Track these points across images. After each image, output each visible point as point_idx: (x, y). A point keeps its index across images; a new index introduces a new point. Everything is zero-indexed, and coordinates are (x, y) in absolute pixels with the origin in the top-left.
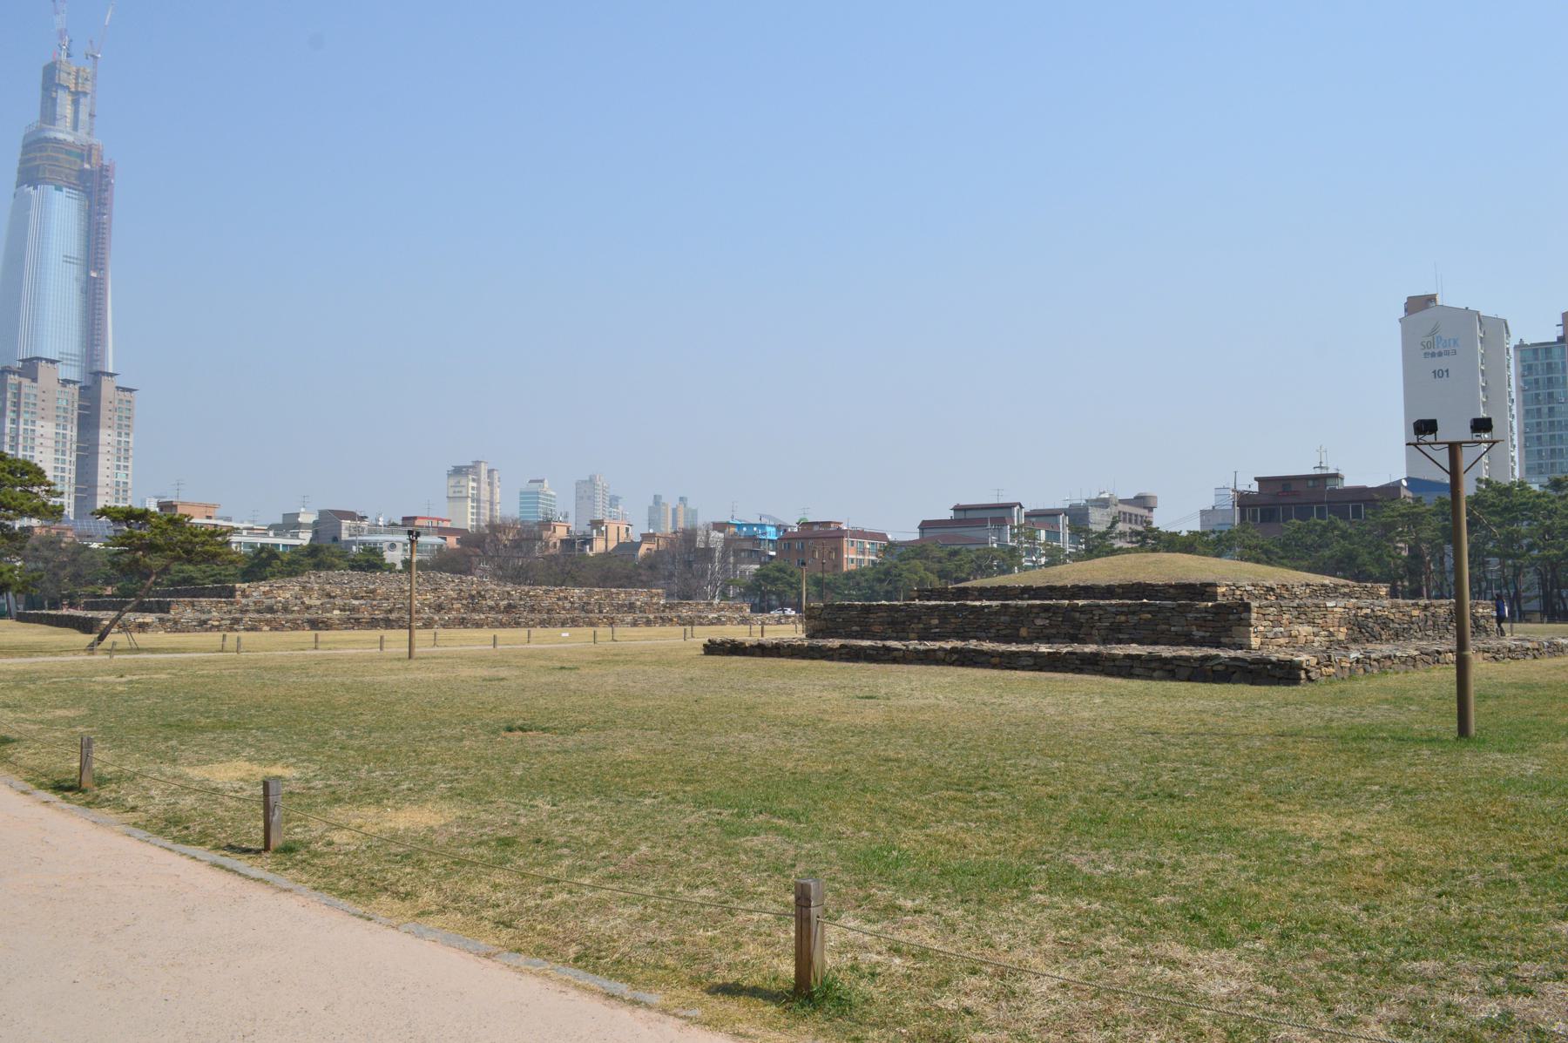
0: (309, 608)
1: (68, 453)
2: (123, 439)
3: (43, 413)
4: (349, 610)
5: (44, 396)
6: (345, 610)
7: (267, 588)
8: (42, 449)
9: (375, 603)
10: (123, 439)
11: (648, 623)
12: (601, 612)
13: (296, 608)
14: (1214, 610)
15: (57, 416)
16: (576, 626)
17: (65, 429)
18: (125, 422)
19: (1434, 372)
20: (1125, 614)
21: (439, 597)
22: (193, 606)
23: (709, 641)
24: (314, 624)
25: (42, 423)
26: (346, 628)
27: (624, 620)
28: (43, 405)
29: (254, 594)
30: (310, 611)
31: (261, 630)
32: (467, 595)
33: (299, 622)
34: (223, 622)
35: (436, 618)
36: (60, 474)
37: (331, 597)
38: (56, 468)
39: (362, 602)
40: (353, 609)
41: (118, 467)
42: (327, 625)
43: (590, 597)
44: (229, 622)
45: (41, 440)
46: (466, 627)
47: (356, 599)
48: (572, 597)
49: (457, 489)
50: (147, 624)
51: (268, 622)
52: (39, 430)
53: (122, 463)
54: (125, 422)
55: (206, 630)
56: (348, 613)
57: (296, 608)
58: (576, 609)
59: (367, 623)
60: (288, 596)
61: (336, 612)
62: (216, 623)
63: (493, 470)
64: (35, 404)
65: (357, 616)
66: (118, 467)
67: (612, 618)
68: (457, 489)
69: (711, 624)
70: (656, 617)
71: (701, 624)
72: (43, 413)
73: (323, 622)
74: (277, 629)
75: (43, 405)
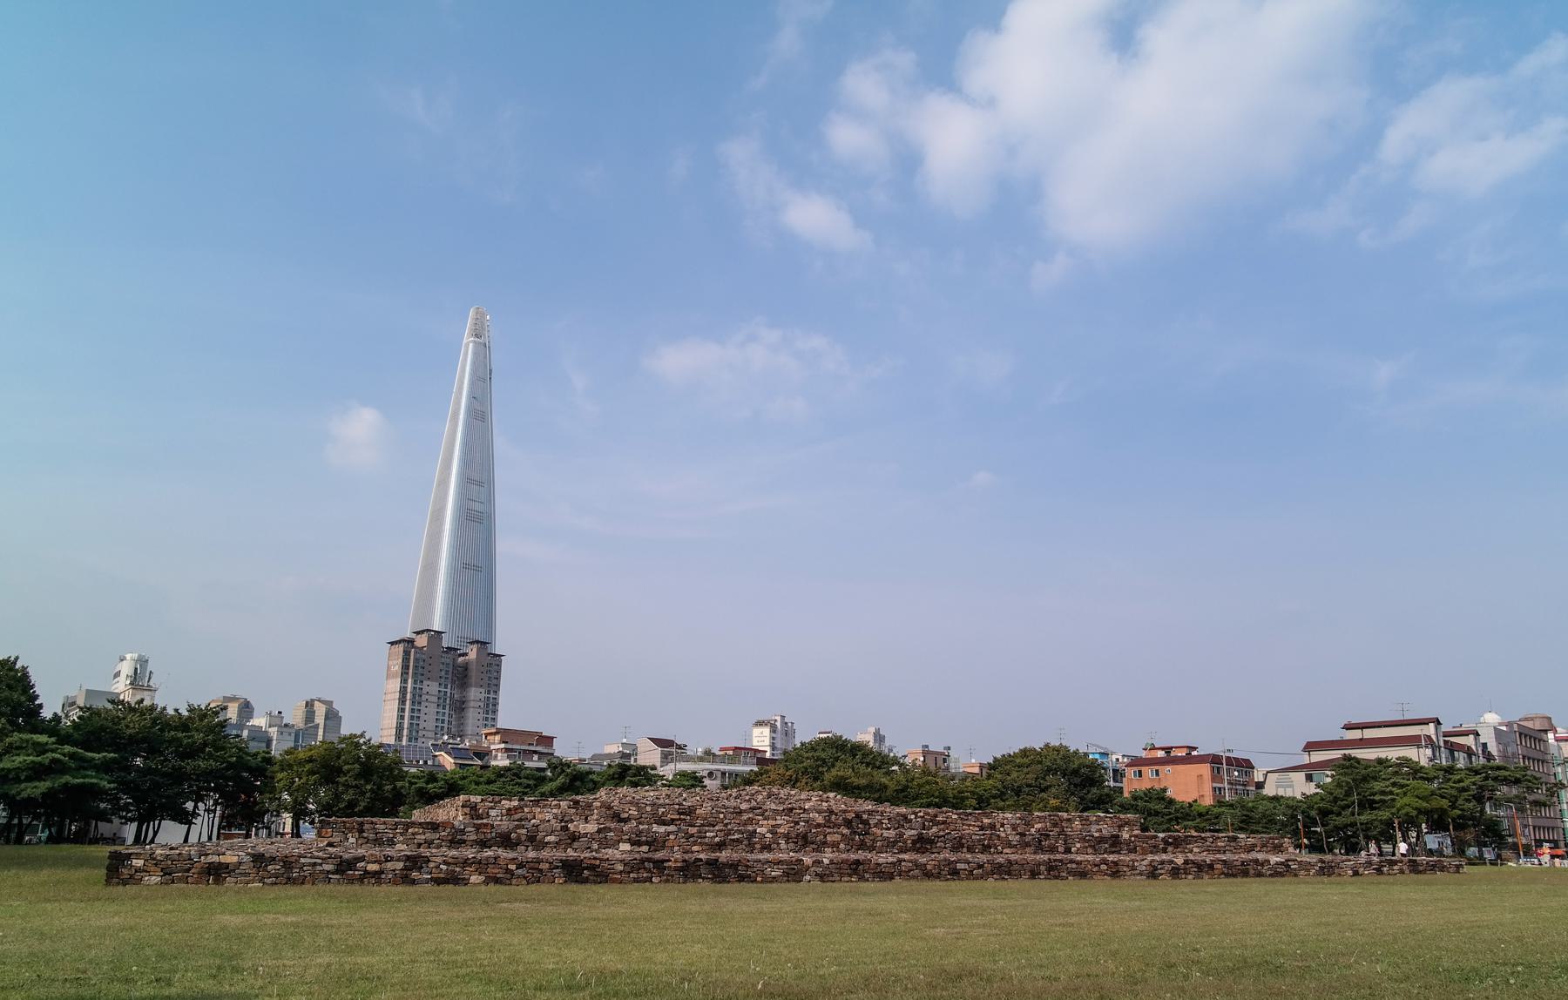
0: (574, 838)
1: (448, 707)
2: (492, 695)
3: (429, 675)
4: (647, 843)
5: (430, 661)
6: (639, 844)
7: (516, 803)
8: (427, 704)
9: (693, 830)
10: (492, 695)
11: (1176, 872)
12: (1068, 851)
13: (551, 838)
14: (450, 838)
15: (441, 677)
16: (1056, 877)
17: (446, 687)
18: (495, 681)
19: (949, 748)
20: (1220, 830)
21: (797, 823)
22: (361, 831)
23: (38, 696)
24: (574, 872)
25: (428, 683)
26: (636, 881)
27: (1133, 868)
28: (430, 668)
29: (493, 813)
30: (576, 845)
31: (466, 882)
32: (840, 821)
33: (545, 866)
34: (389, 865)
35: (808, 860)
36: (440, 725)
37: (621, 820)
38: (437, 719)
39: (672, 828)
40: (655, 843)
41: (487, 719)
42: (597, 874)
43: (1028, 824)
44: (400, 865)
45: (424, 733)
46: (862, 879)
47: (664, 823)
48: (1003, 825)
49: (760, 739)
50: (227, 865)
51: (481, 866)
52: (426, 689)
53: (490, 716)
54: (495, 681)
55: (351, 881)
56: (645, 848)
57: (551, 838)
58: (1028, 845)
59: (676, 869)
60: (548, 816)
61: (625, 847)
62: (373, 867)
63: (313, 700)
64: (423, 675)
65: (659, 855)
66: (487, 719)
67: (1116, 863)
68: (760, 739)
69: (1276, 874)
70: (1186, 862)
71: (1259, 875)
72: (429, 675)
73: (592, 868)
74: (497, 881)
75: (430, 668)
